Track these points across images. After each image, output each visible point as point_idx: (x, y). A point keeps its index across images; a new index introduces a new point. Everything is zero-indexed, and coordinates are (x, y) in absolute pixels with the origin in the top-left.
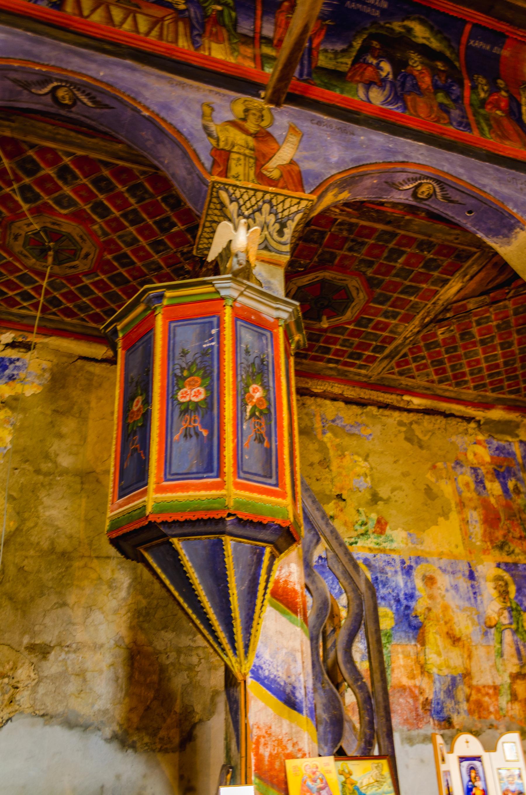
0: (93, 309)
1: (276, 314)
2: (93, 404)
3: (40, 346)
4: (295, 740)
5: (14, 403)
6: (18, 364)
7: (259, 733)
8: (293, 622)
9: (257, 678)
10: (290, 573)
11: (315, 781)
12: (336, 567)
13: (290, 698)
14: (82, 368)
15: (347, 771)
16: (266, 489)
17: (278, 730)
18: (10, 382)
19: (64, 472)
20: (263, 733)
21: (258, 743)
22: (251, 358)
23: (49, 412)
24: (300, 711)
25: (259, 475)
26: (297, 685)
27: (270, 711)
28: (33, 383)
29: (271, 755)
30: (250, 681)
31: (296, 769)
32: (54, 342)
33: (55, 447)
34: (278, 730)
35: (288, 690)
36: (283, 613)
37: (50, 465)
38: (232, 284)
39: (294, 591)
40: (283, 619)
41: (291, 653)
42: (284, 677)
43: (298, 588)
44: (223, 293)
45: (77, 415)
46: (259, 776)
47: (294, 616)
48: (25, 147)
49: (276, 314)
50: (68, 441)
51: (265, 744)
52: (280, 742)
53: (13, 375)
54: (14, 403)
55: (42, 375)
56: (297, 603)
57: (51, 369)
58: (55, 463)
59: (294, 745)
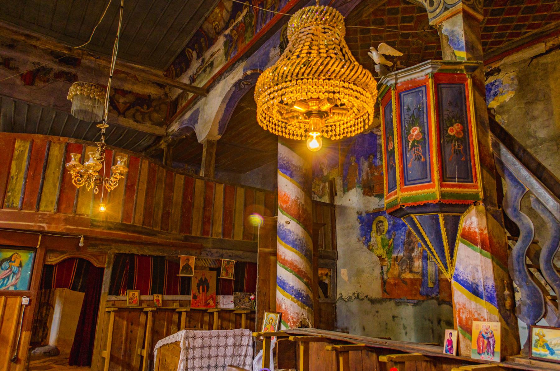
0: (506, 33)
1: (423, 73)
2: (552, 86)
3: (502, 66)
4: (479, 312)
5: (501, 110)
6: (496, 84)
7: (460, 307)
8: (475, 250)
9: (457, 280)
10: (472, 223)
11: (487, 333)
12: (537, 207)
13: (475, 291)
14: (537, 64)
15: (541, 334)
16: (421, 186)
17: (470, 306)
18: (496, 98)
19: (544, 141)
20: (461, 307)
21: (459, 311)
22: (411, 113)
23: (523, 106)
24: (482, 298)
25: (419, 179)
26: (479, 284)
27: (465, 297)
28: (508, 91)
29: (466, 318)
30: (453, 282)
31: (477, 327)
32: (508, 60)
33: (533, 127)
34: (470, 306)
35: (474, 286)
36: (469, 245)
37: (532, 140)
38: (388, 79)
39: (475, 232)
40: (469, 249)
41: (475, 268)
42: (472, 280)
43: (477, 230)
44: (389, 84)
45: (543, 99)
46: (461, 327)
47: (475, 246)
48: (382, 8)
49: (423, 73)
50: (540, 120)
51: (463, 312)
52: (471, 312)
53: (496, 92)
54: (501, 110)
55: (513, 83)
56: (477, 239)
57: (517, 76)
58: (535, 137)
59: (478, 314)
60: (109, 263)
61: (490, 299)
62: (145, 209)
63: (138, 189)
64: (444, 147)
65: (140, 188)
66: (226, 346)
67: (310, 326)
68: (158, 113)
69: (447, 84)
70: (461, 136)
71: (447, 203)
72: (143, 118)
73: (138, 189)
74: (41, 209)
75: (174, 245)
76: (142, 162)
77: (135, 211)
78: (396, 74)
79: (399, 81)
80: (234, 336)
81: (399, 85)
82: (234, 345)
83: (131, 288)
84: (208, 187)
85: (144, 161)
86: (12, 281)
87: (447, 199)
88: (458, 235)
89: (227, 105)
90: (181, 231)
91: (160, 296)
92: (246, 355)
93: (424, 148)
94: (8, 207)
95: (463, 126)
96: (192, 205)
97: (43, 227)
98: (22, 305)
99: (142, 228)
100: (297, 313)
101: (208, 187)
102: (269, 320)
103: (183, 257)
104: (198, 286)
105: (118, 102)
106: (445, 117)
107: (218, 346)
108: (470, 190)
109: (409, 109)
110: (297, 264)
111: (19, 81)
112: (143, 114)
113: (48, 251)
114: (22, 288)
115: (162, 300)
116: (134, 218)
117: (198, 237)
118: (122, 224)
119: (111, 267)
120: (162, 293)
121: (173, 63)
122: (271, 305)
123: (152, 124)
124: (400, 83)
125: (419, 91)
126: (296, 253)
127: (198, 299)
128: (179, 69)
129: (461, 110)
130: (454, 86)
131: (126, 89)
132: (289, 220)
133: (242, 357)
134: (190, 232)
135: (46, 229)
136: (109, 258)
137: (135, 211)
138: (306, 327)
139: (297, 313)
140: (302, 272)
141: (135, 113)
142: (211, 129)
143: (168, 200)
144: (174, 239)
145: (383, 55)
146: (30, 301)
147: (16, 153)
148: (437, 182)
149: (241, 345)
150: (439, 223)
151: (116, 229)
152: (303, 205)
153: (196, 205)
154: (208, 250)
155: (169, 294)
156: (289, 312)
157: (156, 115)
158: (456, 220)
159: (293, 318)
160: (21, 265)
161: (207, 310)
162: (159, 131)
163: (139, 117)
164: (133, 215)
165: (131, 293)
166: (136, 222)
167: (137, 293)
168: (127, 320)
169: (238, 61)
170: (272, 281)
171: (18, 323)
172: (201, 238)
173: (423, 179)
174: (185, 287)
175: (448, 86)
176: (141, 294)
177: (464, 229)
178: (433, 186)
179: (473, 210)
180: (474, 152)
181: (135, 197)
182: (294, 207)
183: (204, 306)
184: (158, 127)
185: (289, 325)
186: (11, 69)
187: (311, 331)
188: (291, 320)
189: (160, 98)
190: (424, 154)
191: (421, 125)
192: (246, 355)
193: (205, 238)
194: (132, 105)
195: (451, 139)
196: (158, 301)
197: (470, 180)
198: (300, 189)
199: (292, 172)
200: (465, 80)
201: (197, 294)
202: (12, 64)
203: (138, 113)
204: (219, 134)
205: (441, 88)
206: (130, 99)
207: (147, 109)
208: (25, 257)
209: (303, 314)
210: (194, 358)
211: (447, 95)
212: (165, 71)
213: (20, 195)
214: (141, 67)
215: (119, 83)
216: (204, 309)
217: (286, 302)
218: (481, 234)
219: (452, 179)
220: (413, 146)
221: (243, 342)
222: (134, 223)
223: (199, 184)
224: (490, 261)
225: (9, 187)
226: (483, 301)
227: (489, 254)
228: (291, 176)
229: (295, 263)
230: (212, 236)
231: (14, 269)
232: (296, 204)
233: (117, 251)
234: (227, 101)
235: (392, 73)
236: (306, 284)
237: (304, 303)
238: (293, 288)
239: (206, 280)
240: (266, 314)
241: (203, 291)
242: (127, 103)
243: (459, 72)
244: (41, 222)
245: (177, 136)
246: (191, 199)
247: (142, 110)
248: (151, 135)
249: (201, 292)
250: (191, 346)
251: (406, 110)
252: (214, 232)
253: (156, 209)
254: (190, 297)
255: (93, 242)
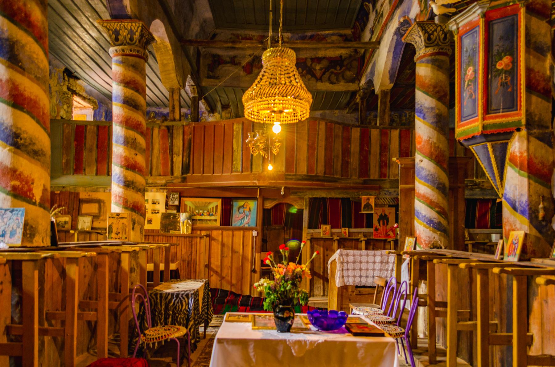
1: (476, 15)
22: (468, 54)
39: (517, 156)
60: (306, 205)
61: (523, 213)
62: (326, 162)
63: (318, 146)
64: (491, 82)
65: (319, 145)
66: (374, 262)
67: (443, 248)
68: (349, 71)
69: (499, 19)
70: (510, 68)
71: (489, 133)
72: (337, 79)
73: (318, 146)
74: (253, 170)
75: (354, 188)
76: (319, 124)
77: (317, 164)
78: (455, 20)
79: (460, 25)
80: (382, 255)
81: (460, 29)
82: (382, 262)
83: (325, 223)
84: (384, 134)
85: (321, 122)
86: (246, 220)
87: (489, 130)
88: (507, 160)
89: (393, 53)
90: (360, 176)
91: (347, 229)
92: (392, 270)
93: (475, 86)
94: (235, 172)
95: (514, 59)
96: (368, 152)
97: (255, 183)
98: (253, 236)
99: (324, 177)
100: (429, 237)
101: (384, 134)
102: (409, 243)
103: (364, 197)
104: (379, 221)
105: (315, 70)
106: (495, 52)
107: (367, 262)
108: (513, 118)
109: (467, 51)
110: (429, 196)
111: (242, 73)
112: (336, 74)
113: (265, 199)
114: (253, 225)
115: (349, 233)
116: (317, 169)
117: (376, 180)
118: (307, 176)
119: (308, 208)
120: (350, 227)
121: (357, 19)
122: (411, 233)
123: (345, 82)
124: (461, 26)
125: (474, 32)
126: (428, 186)
127: (379, 231)
128: (362, 24)
129: (512, 42)
130: (506, 19)
131: (320, 56)
132: (422, 158)
133: (389, 272)
134: (369, 176)
135: (258, 184)
136: (306, 202)
137: (317, 164)
138: (438, 248)
139: (429, 237)
140: (434, 202)
141: (330, 76)
142: (382, 80)
143: (346, 152)
144: (354, 183)
145: (443, 5)
146: (258, 233)
147: (235, 133)
148: (480, 116)
149: (388, 262)
150: (488, 152)
151: (306, 180)
152: (435, 143)
153: (372, 152)
154: (386, 190)
155: (356, 227)
156: (422, 236)
157: (348, 73)
158: (504, 148)
159: (425, 241)
160: (250, 210)
161: (387, 240)
162: (352, 87)
163: (333, 78)
164: (315, 168)
165: (324, 227)
166: (318, 172)
167: (328, 227)
168: (323, 247)
169: (396, 9)
170: (411, 212)
171: (253, 248)
172: (379, 180)
173: (473, 114)
174: (368, 221)
175: (500, 20)
176: (332, 228)
177: (511, 153)
178: (477, 120)
179: (517, 135)
180: (520, 81)
181: (315, 153)
182: (426, 146)
183: (385, 237)
184: (351, 84)
185: (422, 246)
186: (235, 64)
187: (443, 251)
188: (423, 243)
189: (350, 56)
190: (475, 91)
191: (474, 66)
192: (392, 270)
193: (382, 180)
194: (327, 69)
195: (499, 72)
196: (345, 233)
197: (515, 108)
198: (432, 130)
199: (424, 115)
200: (518, 10)
201: (379, 227)
202: (236, 60)
203: (333, 75)
204: (391, 83)
205: (493, 24)
206: (325, 63)
207: (340, 69)
208: (252, 205)
209: (434, 238)
210: (348, 270)
211: (498, 30)
212: (352, 29)
213: (241, 163)
214: (331, 32)
215: (315, 52)
216: (384, 239)
217: (422, 230)
218: (521, 157)
219: (497, 110)
220: (468, 85)
221: (389, 260)
222: (317, 173)
223: (375, 133)
224: (525, 181)
225: (234, 158)
226: (518, 214)
227: (526, 174)
228: (424, 118)
229: (427, 195)
230: (389, 177)
231: (247, 213)
232: (428, 143)
233: (310, 196)
234: (393, 50)
235: (452, 20)
236: (439, 213)
237: (435, 228)
238: (425, 216)
239: (385, 215)
240: (407, 238)
241: (384, 224)
242: (323, 68)
243: (511, 4)
244: (254, 180)
245: (366, 89)
246: (368, 147)
247: (336, 71)
248: (346, 92)
249: (381, 225)
250: (345, 261)
251: (465, 52)
252: (391, 173)
253: (335, 160)
254: (372, 230)
255: (294, 191)
